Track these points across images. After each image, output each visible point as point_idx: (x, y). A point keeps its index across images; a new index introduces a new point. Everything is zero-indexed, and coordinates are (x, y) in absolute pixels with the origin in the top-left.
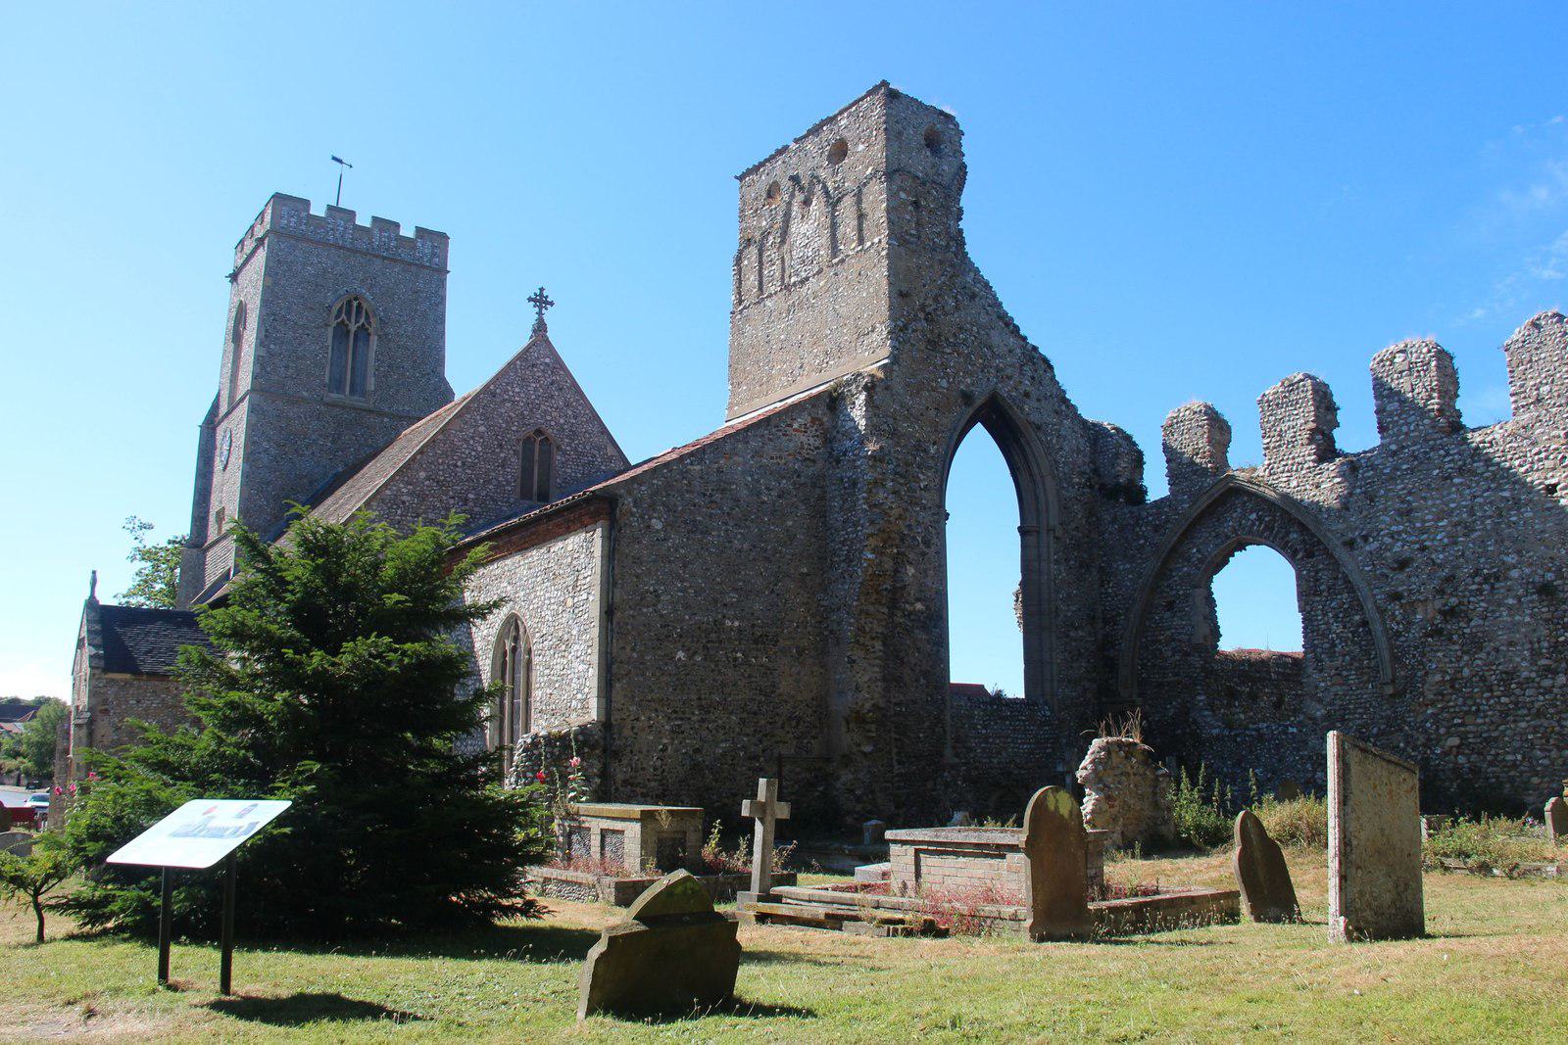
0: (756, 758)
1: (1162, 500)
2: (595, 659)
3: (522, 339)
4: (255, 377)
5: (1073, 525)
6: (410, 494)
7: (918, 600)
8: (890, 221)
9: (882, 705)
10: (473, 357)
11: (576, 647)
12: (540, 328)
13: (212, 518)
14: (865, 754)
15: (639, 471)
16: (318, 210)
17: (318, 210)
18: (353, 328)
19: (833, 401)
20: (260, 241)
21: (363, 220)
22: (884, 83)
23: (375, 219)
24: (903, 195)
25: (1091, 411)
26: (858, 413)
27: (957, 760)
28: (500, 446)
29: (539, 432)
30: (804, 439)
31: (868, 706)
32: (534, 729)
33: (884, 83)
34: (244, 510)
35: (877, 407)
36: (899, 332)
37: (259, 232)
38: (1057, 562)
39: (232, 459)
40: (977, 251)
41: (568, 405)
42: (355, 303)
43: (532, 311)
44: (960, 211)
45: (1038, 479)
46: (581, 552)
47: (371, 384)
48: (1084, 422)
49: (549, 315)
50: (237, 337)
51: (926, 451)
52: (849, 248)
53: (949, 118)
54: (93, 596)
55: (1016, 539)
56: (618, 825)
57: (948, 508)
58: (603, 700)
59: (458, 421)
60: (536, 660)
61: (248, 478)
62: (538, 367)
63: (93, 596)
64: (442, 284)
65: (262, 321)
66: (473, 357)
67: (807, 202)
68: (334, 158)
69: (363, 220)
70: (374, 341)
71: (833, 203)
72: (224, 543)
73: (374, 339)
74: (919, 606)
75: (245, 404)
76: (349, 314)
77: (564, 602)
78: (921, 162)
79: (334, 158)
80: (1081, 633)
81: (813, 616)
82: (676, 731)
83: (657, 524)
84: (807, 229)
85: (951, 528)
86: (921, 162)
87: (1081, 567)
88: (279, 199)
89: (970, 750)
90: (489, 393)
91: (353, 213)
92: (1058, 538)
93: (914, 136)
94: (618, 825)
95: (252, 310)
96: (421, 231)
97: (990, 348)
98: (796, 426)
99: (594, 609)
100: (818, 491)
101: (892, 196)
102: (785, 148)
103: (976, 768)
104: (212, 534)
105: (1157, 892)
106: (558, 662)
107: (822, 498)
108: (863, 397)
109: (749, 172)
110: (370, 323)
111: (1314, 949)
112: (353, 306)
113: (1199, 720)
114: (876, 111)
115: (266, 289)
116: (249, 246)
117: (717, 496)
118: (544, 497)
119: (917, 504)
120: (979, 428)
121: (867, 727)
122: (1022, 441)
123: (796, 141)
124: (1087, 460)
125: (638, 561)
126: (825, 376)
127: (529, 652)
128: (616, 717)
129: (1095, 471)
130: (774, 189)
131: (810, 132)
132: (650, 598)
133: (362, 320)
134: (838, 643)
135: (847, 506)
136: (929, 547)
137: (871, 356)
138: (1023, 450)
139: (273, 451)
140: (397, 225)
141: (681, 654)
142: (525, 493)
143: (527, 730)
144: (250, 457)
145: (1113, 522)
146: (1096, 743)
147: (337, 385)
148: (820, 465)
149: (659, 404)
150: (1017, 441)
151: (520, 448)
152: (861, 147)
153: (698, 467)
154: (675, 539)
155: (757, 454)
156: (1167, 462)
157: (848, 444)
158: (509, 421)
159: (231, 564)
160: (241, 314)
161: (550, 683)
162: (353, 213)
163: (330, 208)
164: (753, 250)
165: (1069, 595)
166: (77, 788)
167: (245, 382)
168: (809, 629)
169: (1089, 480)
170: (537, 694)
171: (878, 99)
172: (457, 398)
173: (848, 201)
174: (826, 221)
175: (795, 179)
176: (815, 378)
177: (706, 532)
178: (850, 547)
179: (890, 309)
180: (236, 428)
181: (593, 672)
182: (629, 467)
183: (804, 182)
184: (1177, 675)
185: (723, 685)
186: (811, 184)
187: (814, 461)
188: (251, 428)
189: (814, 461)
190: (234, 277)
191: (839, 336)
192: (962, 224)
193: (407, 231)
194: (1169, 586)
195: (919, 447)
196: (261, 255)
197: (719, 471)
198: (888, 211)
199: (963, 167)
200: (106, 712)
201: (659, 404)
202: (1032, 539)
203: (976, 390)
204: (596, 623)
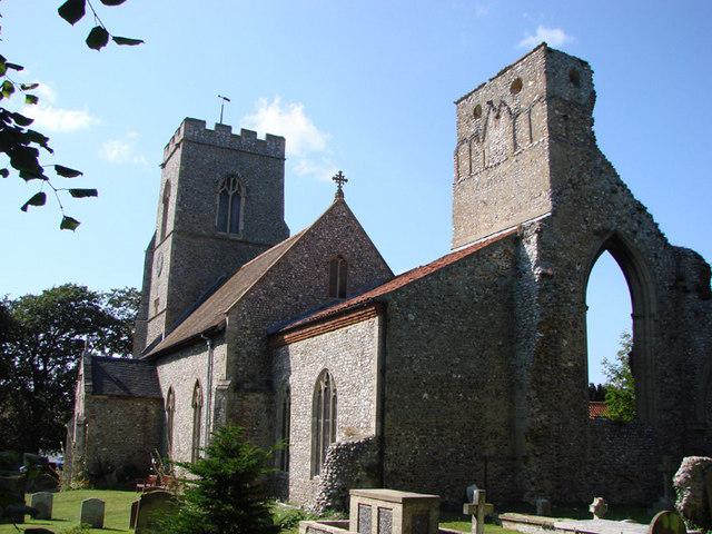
0: (470, 457)
2: (374, 398)
3: (329, 202)
4: (176, 223)
8: (550, 129)
10: (301, 211)
12: (340, 194)
13: (152, 303)
15: (404, 281)
16: (210, 126)
17: (210, 126)
18: (231, 193)
19: (516, 239)
20: (178, 146)
21: (236, 131)
22: (544, 44)
23: (268, 136)
24: (557, 112)
25: (675, 238)
26: (531, 249)
32: (338, 440)
33: (544, 44)
34: (170, 301)
36: (557, 195)
37: (177, 140)
38: (655, 336)
39: (163, 270)
40: (605, 143)
41: (356, 240)
44: (593, 119)
46: (365, 334)
47: (241, 228)
49: (345, 188)
50: (166, 201)
51: (574, 269)
52: (524, 145)
53: (584, 64)
56: (389, 505)
60: (339, 397)
61: (172, 282)
62: (339, 218)
65: (180, 191)
66: (301, 211)
67: (498, 117)
69: (236, 131)
70: (243, 200)
71: (514, 116)
72: (158, 318)
73: (243, 199)
74: (570, 364)
75: (170, 239)
76: (229, 184)
77: (356, 363)
78: (567, 92)
82: (422, 442)
83: (411, 317)
84: (498, 133)
86: (567, 92)
88: (188, 121)
89: (602, 453)
90: (310, 235)
91: (230, 128)
93: (563, 75)
94: (389, 505)
95: (300, 439)
96: (269, 136)
97: (612, 204)
98: (494, 255)
99: (374, 368)
101: (550, 112)
104: (152, 312)
106: (353, 400)
107: (511, 299)
108: (535, 237)
109: (462, 99)
112: (230, 179)
114: (540, 61)
115: (181, 172)
116: (172, 148)
117: (448, 300)
118: (343, 296)
119: (569, 301)
123: (491, 80)
125: (400, 339)
126: (511, 223)
127: (335, 391)
130: (476, 113)
131: (499, 75)
132: (408, 361)
134: (521, 388)
137: (539, 207)
139: (186, 266)
141: (426, 395)
142: (332, 294)
143: (334, 440)
144: (173, 270)
146: (686, 460)
149: (412, 238)
151: (329, 266)
152: (531, 83)
154: (422, 325)
155: (471, 273)
158: (323, 251)
159: (163, 330)
160: (168, 184)
161: (347, 412)
162: (230, 128)
163: (217, 125)
164: (466, 146)
167: (170, 227)
170: (340, 417)
171: (541, 53)
172: (292, 234)
173: (523, 116)
174: (511, 128)
175: (490, 103)
176: (505, 224)
177: (441, 321)
179: (551, 181)
180: (165, 252)
181: (374, 406)
182: (392, 277)
183: (496, 105)
186: (500, 106)
187: (506, 277)
188: (175, 254)
189: (506, 277)
191: (521, 198)
192: (593, 128)
195: (570, 267)
196: (179, 151)
197: (449, 284)
198: (549, 122)
201: (412, 238)
202: (639, 322)
203: (494, 98)
204: (376, 376)
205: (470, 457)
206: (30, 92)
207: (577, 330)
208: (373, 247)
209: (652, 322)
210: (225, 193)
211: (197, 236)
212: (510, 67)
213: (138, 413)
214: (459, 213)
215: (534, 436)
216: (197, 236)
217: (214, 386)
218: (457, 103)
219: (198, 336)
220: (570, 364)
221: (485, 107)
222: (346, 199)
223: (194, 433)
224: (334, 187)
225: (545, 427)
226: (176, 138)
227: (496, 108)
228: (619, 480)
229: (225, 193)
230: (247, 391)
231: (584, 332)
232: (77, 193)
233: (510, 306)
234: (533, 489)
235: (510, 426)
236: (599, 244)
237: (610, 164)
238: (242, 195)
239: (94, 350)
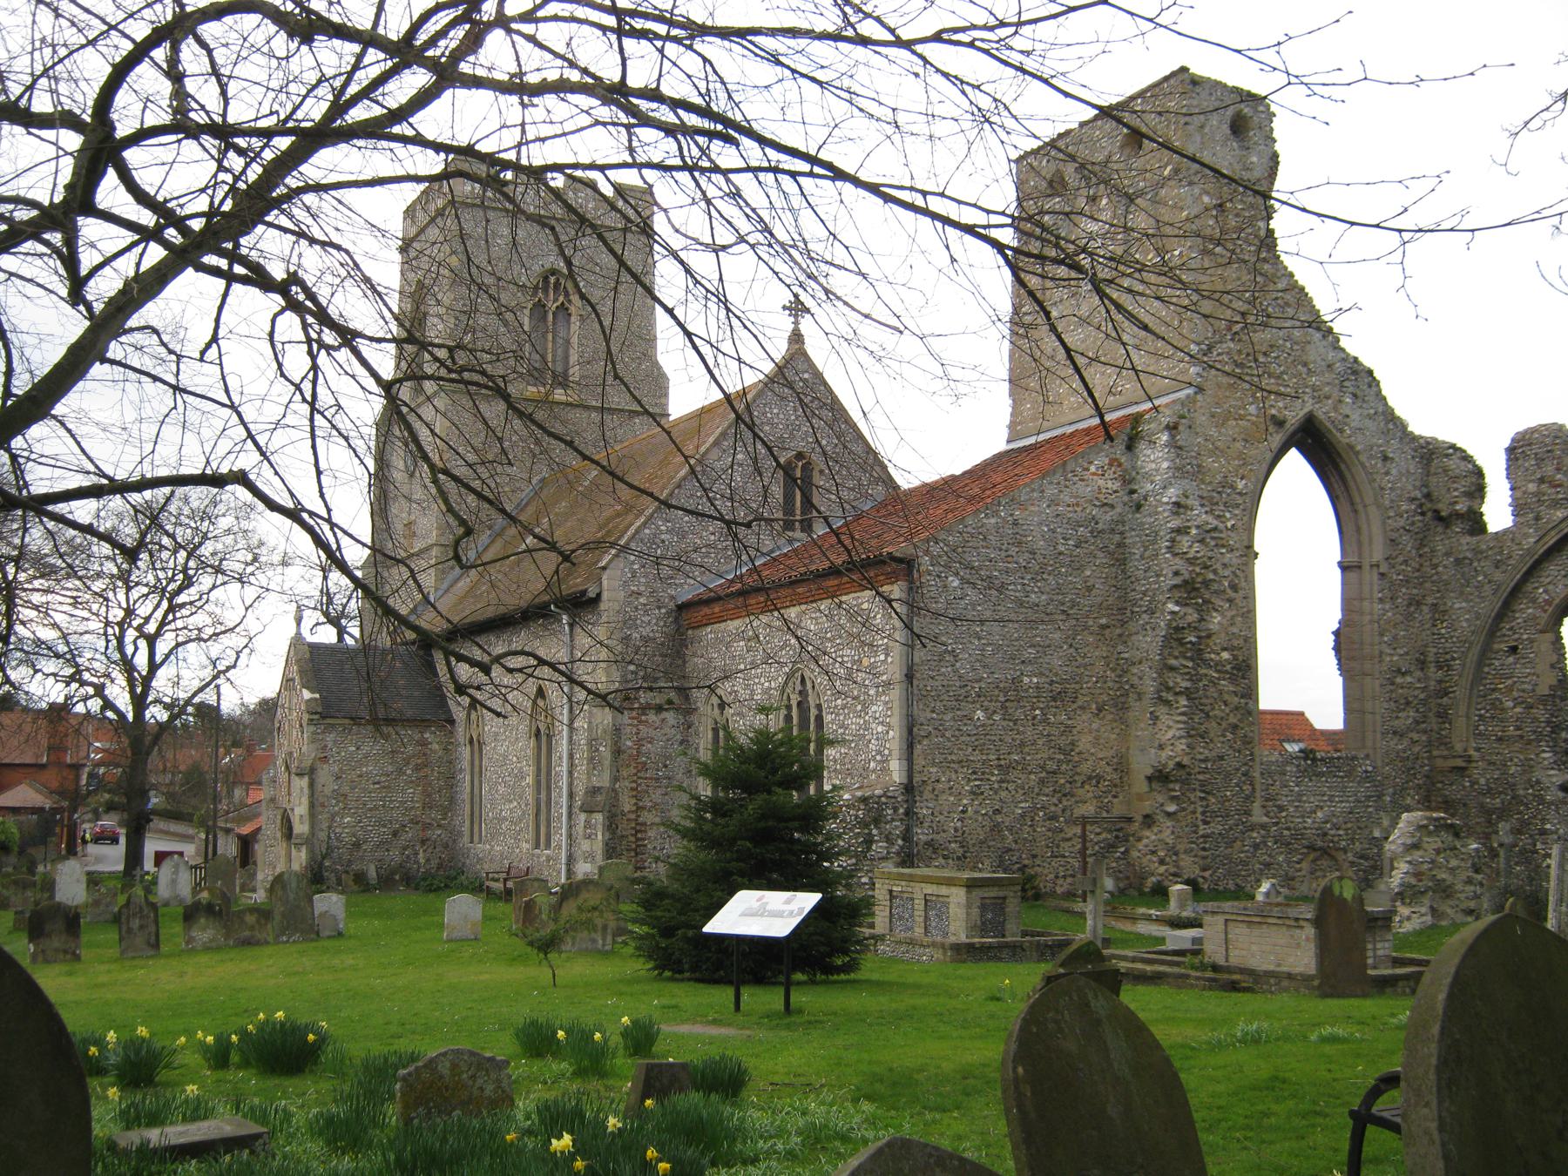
0: (1054, 818)
1: (1505, 531)
5: (1401, 559)
7: (1225, 649)
9: (1186, 761)
11: (874, 708)
12: (796, 337)
14: (1169, 814)
24: (1206, 199)
27: (1265, 819)
30: (1101, 482)
31: (1171, 764)
35: (1180, 448)
42: (552, 280)
45: (1360, 507)
48: (1414, 438)
49: (806, 325)
51: (1233, 487)
54: (298, 634)
55: (1337, 573)
57: (1256, 549)
58: (905, 763)
59: (716, 450)
60: (828, 718)
63: (298, 634)
76: (546, 291)
80: (1409, 679)
81: (1113, 670)
85: (1261, 568)
87: (1410, 604)
89: (1281, 808)
92: (1382, 575)
94: (944, 890)
97: (1305, 364)
98: (1093, 469)
100: (1117, 538)
103: (1288, 829)
105: (789, 707)
108: (1165, 437)
110: (570, 301)
113: (1544, 779)
120: (1294, 458)
121: (1171, 786)
122: (1343, 466)
124: (1418, 484)
127: (819, 707)
128: (917, 779)
129: (1428, 496)
133: (561, 299)
135: (1147, 554)
136: (1236, 591)
141: (980, 714)
145: (1448, 554)
148: (1118, 510)
150: (1337, 467)
153: (993, 521)
155: (1053, 503)
156: (1512, 489)
157: (1149, 487)
165: (1395, 638)
168: (1110, 684)
169: (1421, 506)
178: (1153, 597)
184: (1518, 728)
185: (1022, 744)
187: (1112, 507)
189: (1112, 507)
192: (1273, 224)
194: (1511, 629)
199: (1274, 159)
200: (325, 759)
202: (1353, 575)
205: (1054, 818)
206: (37, 44)
207: (1238, 596)
209: (1376, 577)
215: (1160, 777)
219: (546, 605)
220: (1225, 655)
223: (538, 783)
224: (787, 323)
225: (1180, 765)
228: (1312, 856)
229: (540, 306)
230: (645, 709)
231: (1250, 597)
233: (1120, 558)
234: (1162, 869)
235: (1122, 766)
236: (1277, 439)
237: (1303, 289)
238: (572, 309)
239: (1404, 867)
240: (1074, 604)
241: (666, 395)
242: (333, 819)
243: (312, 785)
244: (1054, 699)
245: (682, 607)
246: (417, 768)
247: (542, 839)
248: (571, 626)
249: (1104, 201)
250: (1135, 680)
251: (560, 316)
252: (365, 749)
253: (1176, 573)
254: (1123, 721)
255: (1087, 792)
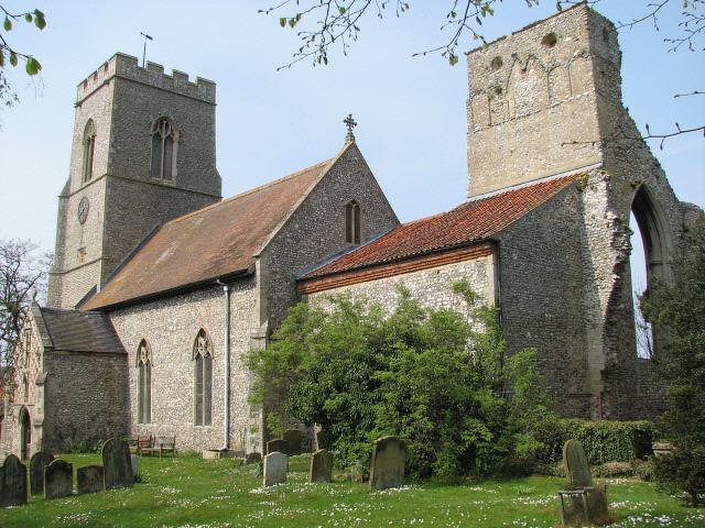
3: (336, 148)
6: (291, 238)
18: (164, 137)
23: (175, 72)
28: (335, 210)
29: (354, 202)
37: (103, 77)
40: (626, 101)
41: (367, 185)
43: (345, 128)
47: (175, 172)
49: (355, 131)
53: (612, 24)
64: (213, 112)
68: (150, 38)
69: (168, 72)
70: (176, 145)
76: (161, 128)
79: (150, 38)
84: (525, 87)
96: (200, 80)
102: (504, 38)
111: (559, 451)
112: (163, 122)
131: (525, 29)
138: (653, 216)
140: (187, 76)
147: (155, 172)
159: (97, 280)
166: (207, 427)
167: (101, 166)
176: (540, 173)
185: (547, 352)
190: (79, 105)
193: (192, 80)
208: (381, 194)
210: (158, 136)
211: (131, 181)
212: (540, 22)
213: (101, 370)
214: (474, 163)
216: (131, 181)
217: (242, 348)
218: (468, 54)
221: (506, 58)
222: (357, 143)
226: (91, 82)
227: (526, 62)
229: (158, 136)
232: (478, 20)
240: (563, 274)
241: (220, 187)
242: (57, 411)
243: (45, 390)
244: (558, 327)
245: (298, 282)
246: (106, 381)
247: (203, 413)
248: (229, 292)
249: (532, 71)
250: (591, 317)
251: (168, 143)
252: (76, 369)
253: (162, 361)
254: (584, 340)
255: (572, 380)
